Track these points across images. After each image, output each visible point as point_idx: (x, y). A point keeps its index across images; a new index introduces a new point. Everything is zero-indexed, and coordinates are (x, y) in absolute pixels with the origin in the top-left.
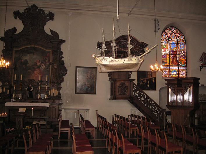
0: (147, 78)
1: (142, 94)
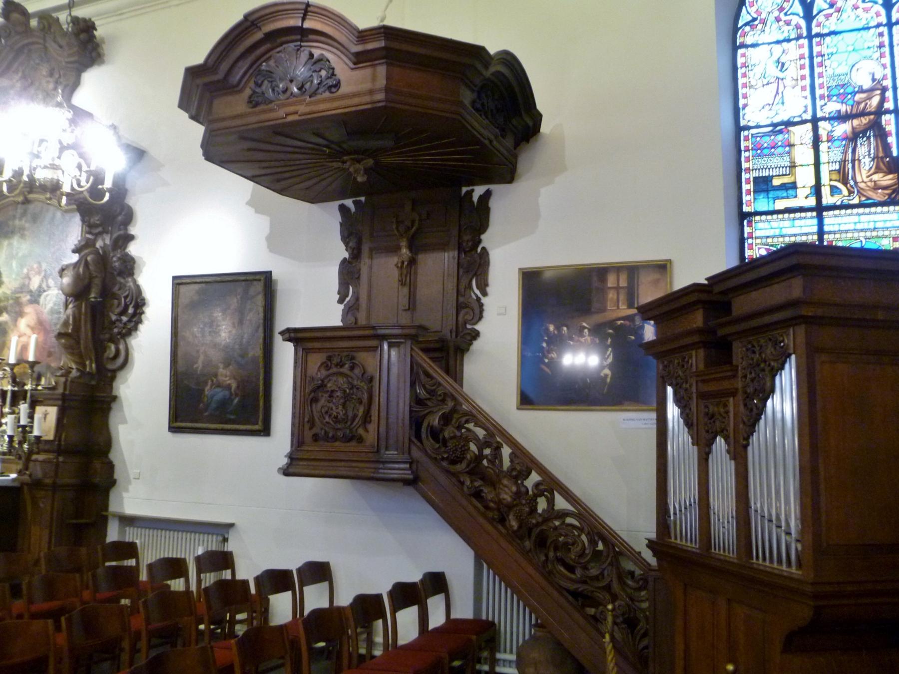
0: (598, 318)
1: (480, 433)
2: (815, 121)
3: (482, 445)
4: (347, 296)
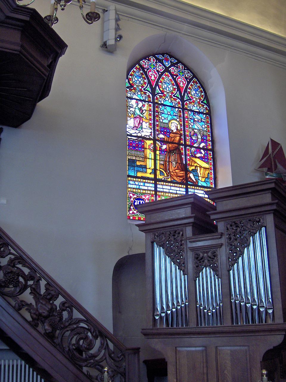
1: (26, 271)
2: (155, 140)
3: (27, 278)
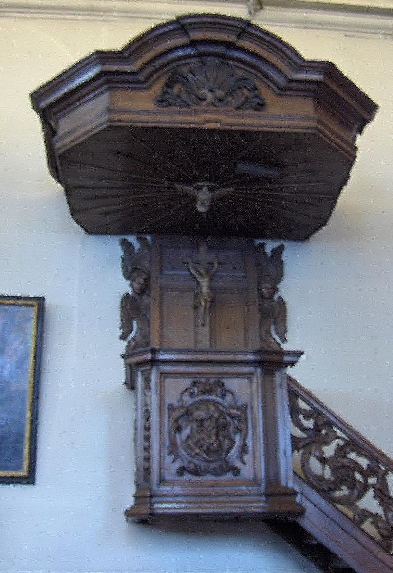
1: (364, 462)
3: (365, 474)
4: (131, 332)
